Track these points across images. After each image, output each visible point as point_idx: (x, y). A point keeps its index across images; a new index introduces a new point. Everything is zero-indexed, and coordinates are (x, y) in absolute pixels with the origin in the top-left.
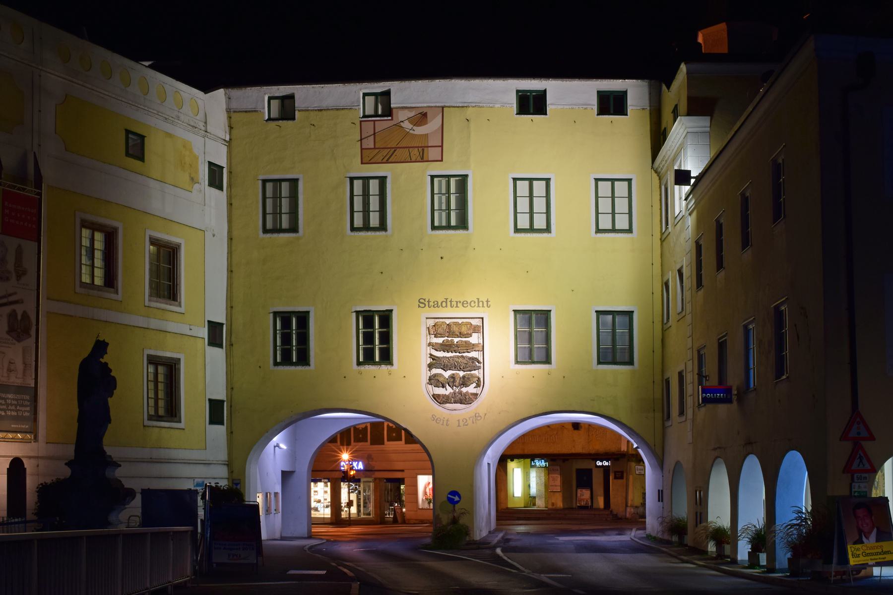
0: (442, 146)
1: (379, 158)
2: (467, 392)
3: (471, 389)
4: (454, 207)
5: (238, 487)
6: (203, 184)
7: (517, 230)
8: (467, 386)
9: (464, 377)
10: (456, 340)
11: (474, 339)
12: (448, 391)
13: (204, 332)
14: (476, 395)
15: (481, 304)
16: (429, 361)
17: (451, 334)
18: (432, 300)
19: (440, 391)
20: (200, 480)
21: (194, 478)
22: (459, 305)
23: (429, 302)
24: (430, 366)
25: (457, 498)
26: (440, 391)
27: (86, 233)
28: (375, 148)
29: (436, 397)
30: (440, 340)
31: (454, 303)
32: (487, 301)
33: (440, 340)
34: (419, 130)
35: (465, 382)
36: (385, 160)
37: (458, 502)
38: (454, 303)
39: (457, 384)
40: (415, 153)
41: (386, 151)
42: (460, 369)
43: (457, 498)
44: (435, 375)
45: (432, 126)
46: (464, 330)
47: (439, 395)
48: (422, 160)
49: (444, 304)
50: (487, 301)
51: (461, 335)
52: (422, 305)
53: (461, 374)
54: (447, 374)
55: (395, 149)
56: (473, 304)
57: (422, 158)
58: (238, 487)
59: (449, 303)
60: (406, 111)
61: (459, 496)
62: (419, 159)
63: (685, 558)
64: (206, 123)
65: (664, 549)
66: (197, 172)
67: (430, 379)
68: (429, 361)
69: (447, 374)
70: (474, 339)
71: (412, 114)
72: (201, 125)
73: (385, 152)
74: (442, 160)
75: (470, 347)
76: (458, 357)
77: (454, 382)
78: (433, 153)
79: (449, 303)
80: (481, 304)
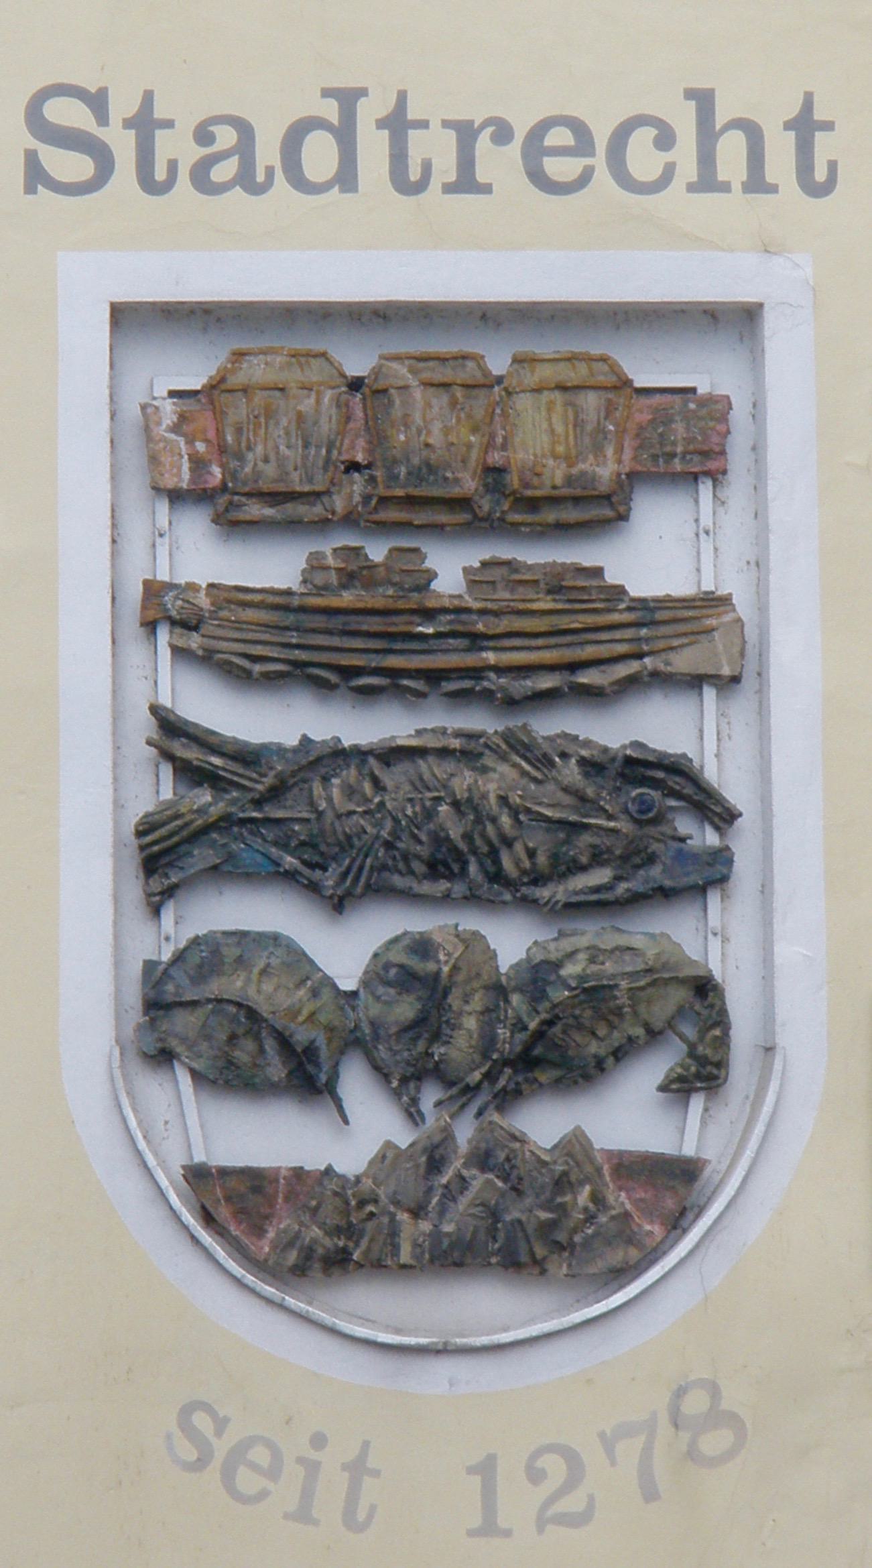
2: (575, 1146)
3: (626, 1114)
8: (582, 1075)
9: (538, 975)
10: (450, 568)
11: (653, 554)
12: (358, 1132)
14: (673, 1184)
15: (731, 153)
16: (152, 790)
17: (425, 502)
18: (182, 107)
19: (270, 1137)
22: (499, 164)
23: (145, 124)
24: (163, 858)
26: (270, 1137)
29: (230, 1203)
30: (275, 566)
31: (434, 149)
33: (275, 566)
35: (558, 1042)
38: (434, 149)
39: (460, 1047)
44: (207, 956)
46: (537, 440)
49: (319, 155)
51: (507, 503)
52: (71, 166)
53: (511, 941)
54: (522, 751)
56: (643, 159)
59: (373, 148)
63: (223, 1213)
65: (216, 761)
67: (156, 1006)
68: (152, 790)
69: (346, 949)
70: (653, 554)
76: (470, 752)
77: (431, 1023)
79: (373, 148)
80: (731, 153)
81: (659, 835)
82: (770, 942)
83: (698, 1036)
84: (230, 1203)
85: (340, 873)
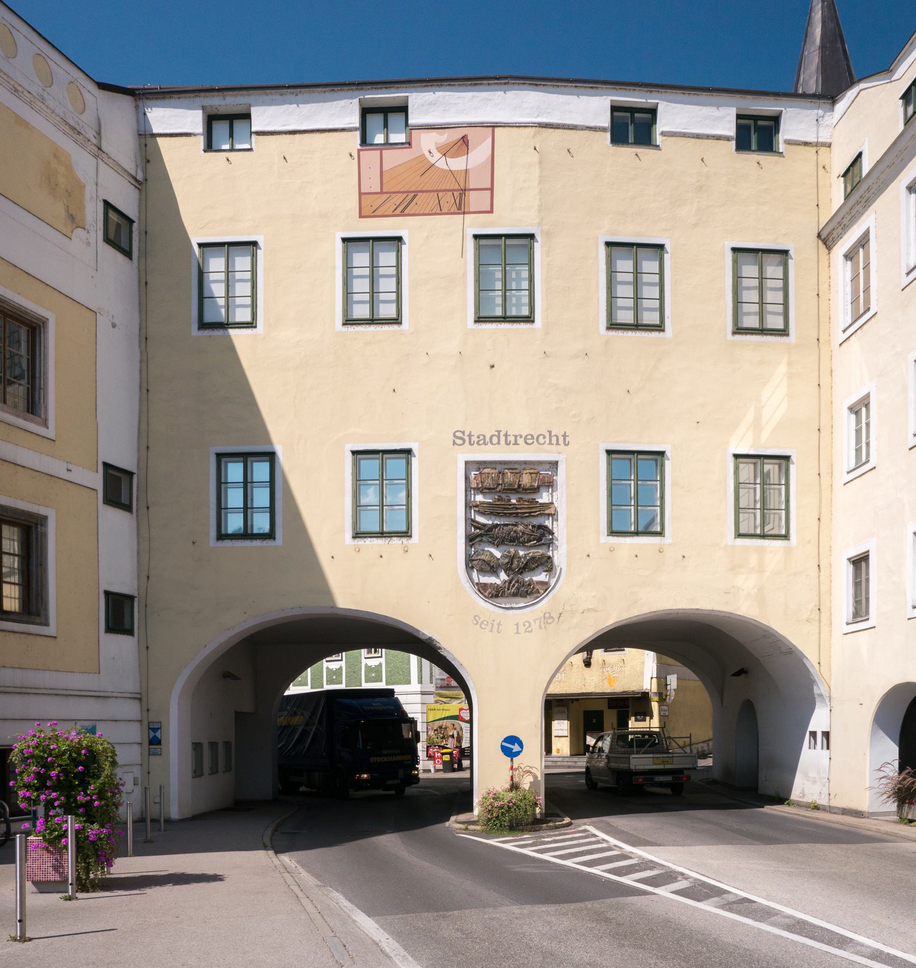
0: (492, 189)
1: (389, 207)
4: (56, 738)
5: (158, 734)
6: (93, 233)
7: (613, 326)
11: (544, 497)
13: (97, 481)
14: (545, 585)
15: (554, 440)
18: (475, 433)
20: (87, 724)
21: (76, 721)
22: (521, 441)
23: (470, 436)
25: (516, 748)
27: (235, 471)
28: (382, 192)
32: (565, 436)
34: (457, 164)
36: (398, 211)
37: (518, 754)
40: (448, 200)
41: (400, 197)
42: (523, 544)
43: (516, 748)
45: (478, 155)
46: (526, 480)
47: (485, 585)
48: (461, 209)
49: (495, 440)
50: (565, 436)
52: (459, 442)
55: (415, 194)
56: (541, 440)
57: (459, 208)
58: (158, 734)
59: (503, 439)
60: (434, 134)
61: (521, 744)
62: (454, 209)
64: (99, 133)
66: (82, 207)
70: (544, 497)
71: (443, 138)
72: (91, 134)
73: (399, 198)
74: (491, 211)
75: (484, 510)
78: (475, 200)
79: (503, 439)
80: (554, 440)
81: (543, 536)
82: (559, 557)
83: (547, 563)
84: (482, 588)
85: (499, 542)
